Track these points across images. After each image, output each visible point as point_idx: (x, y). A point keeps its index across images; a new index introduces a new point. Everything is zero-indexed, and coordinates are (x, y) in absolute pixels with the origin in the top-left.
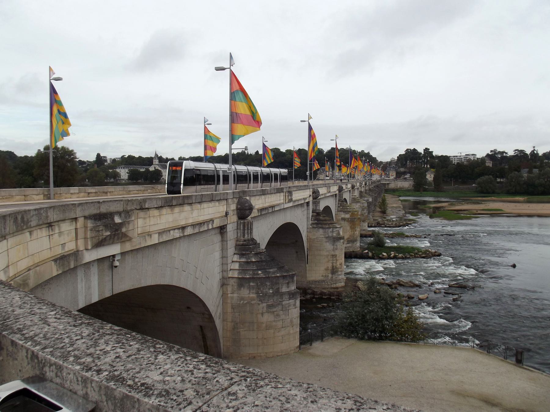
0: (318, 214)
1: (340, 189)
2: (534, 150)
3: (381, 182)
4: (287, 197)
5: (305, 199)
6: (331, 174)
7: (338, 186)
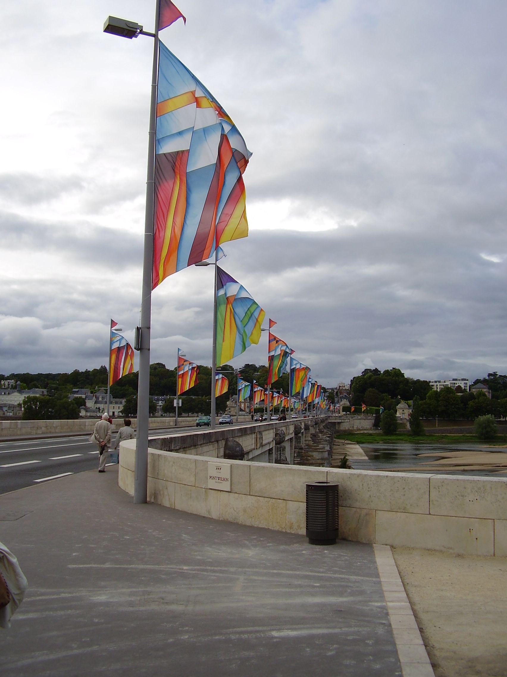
6: (248, 407)
7: (294, 425)
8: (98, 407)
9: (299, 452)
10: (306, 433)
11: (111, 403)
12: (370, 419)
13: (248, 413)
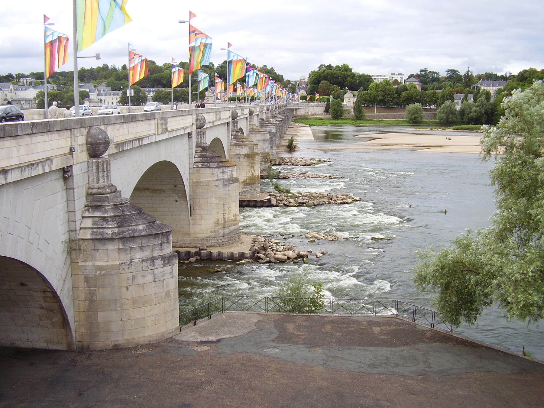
0: (204, 149)
1: (234, 117)
2: (469, 71)
3: (288, 108)
4: (159, 125)
5: (184, 128)
6: (223, 96)
7: (231, 111)
8: (100, 99)
9: (235, 135)
10: (250, 118)
11: (110, 95)
12: (322, 106)
13: (223, 101)
